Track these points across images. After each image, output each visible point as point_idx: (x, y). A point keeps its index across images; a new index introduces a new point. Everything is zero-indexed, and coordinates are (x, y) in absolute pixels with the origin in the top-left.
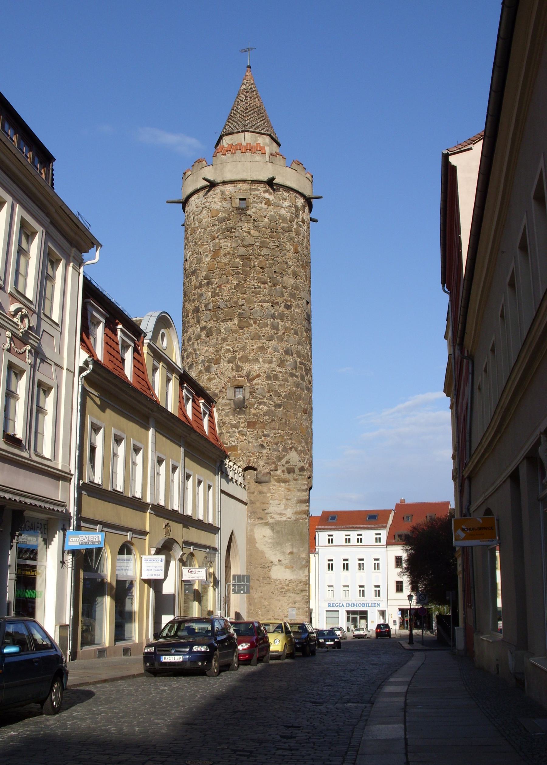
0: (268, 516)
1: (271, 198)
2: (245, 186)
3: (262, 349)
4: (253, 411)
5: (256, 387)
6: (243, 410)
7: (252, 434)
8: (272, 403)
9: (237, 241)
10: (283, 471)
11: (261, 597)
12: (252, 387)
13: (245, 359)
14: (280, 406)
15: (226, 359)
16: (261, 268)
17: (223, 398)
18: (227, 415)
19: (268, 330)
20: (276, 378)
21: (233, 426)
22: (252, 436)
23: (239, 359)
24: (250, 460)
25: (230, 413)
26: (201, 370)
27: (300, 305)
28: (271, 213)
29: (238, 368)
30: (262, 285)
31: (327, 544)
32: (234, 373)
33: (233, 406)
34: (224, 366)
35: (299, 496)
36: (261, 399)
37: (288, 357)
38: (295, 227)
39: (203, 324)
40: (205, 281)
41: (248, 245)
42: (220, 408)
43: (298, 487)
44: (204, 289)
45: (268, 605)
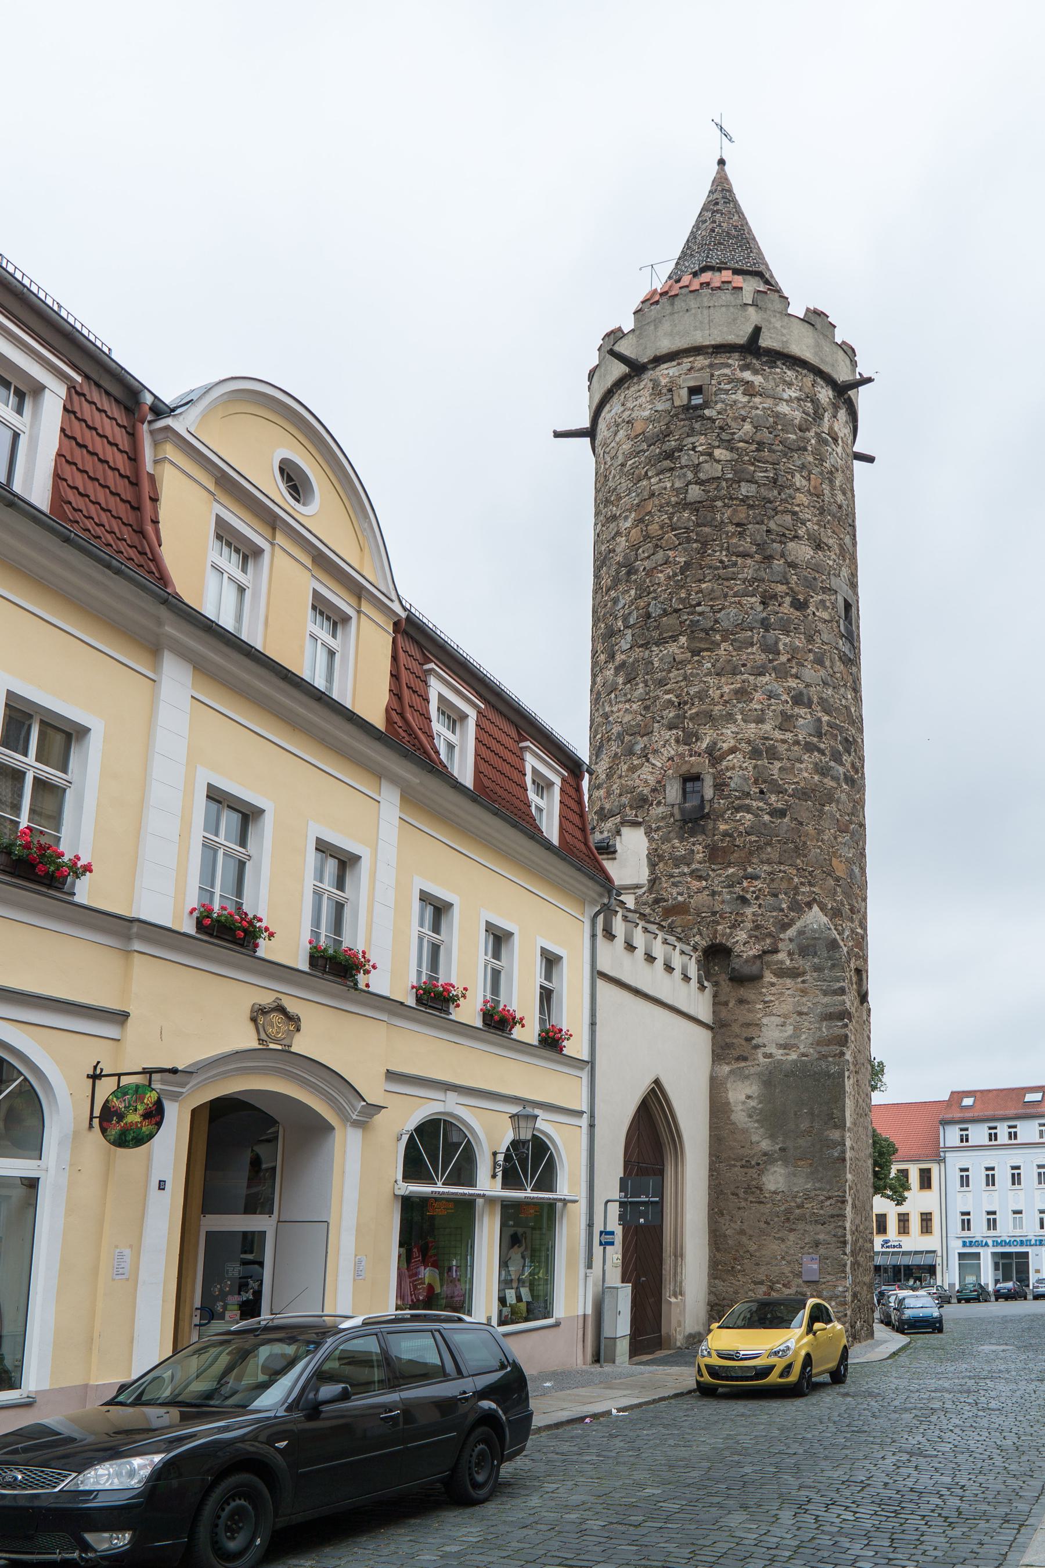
0: (760, 1053)
1: (757, 380)
2: (701, 361)
3: (743, 694)
4: (723, 827)
5: (729, 774)
6: (699, 825)
7: (720, 876)
8: (765, 807)
9: (685, 475)
10: (790, 954)
11: (742, 1232)
13: (709, 717)
14: (782, 813)
15: (665, 722)
16: (738, 525)
17: (659, 803)
18: (665, 840)
19: (756, 655)
20: (773, 755)
21: (678, 862)
22: (720, 879)
23: (691, 719)
24: (716, 931)
25: (671, 835)
26: (616, 754)
27: (828, 604)
28: (758, 412)
29: (689, 738)
30: (740, 560)
33: (678, 817)
34: (662, 735)
35: (826, 1006)
36: (739, 798)
37: (802, 711)
38: (813, 441)
39: (620, 658)
41: (708, 480)
42: (654, 826)
43: (825, 985)
45: (756, 1251)
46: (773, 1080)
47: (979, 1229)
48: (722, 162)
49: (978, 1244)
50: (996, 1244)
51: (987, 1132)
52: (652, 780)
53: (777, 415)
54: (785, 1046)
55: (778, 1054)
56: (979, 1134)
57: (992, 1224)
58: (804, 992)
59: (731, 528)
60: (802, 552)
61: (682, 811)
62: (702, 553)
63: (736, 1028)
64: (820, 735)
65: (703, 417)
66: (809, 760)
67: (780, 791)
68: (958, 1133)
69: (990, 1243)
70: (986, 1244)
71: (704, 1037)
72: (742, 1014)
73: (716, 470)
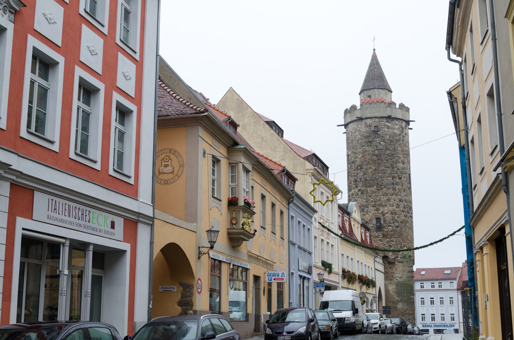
1: (390, 125)
2: (377, 120)
3: (389, 200)
4: (386, 230)
12: (384, 219)
13: (381, 205)
20: (396, 214)
21: (376, 237)
29: (377, 210)
31: (420, 289)
32: (376, 212)
34: (371, 208)
37: (401, 203)
40: (359, 167)
44: (359, 171)
46: (398, 284)
47: (428, 320)
48: (374, 50)
49: (428, 326)
50: (435, 326)
51: (431, 285)
52: (369, 218)
53: (394, 133)
54: (400, 278)
55: (399, 279)
56: (427, 285)
57: (433, 319)
58: (404, 266)
59: (385, 161)
60: (400, 165)
61: (377, 226)
62: (379, 166)
63: (389, 273)
64: (405, 208)
65: (378, 134)
66: (403, 214)
67: (397, 222)
68: (420, 285)
69: (433, 325)
70: (431, 326)
71: (383, 275)
72: (390, 271)
73: (381, 147)
